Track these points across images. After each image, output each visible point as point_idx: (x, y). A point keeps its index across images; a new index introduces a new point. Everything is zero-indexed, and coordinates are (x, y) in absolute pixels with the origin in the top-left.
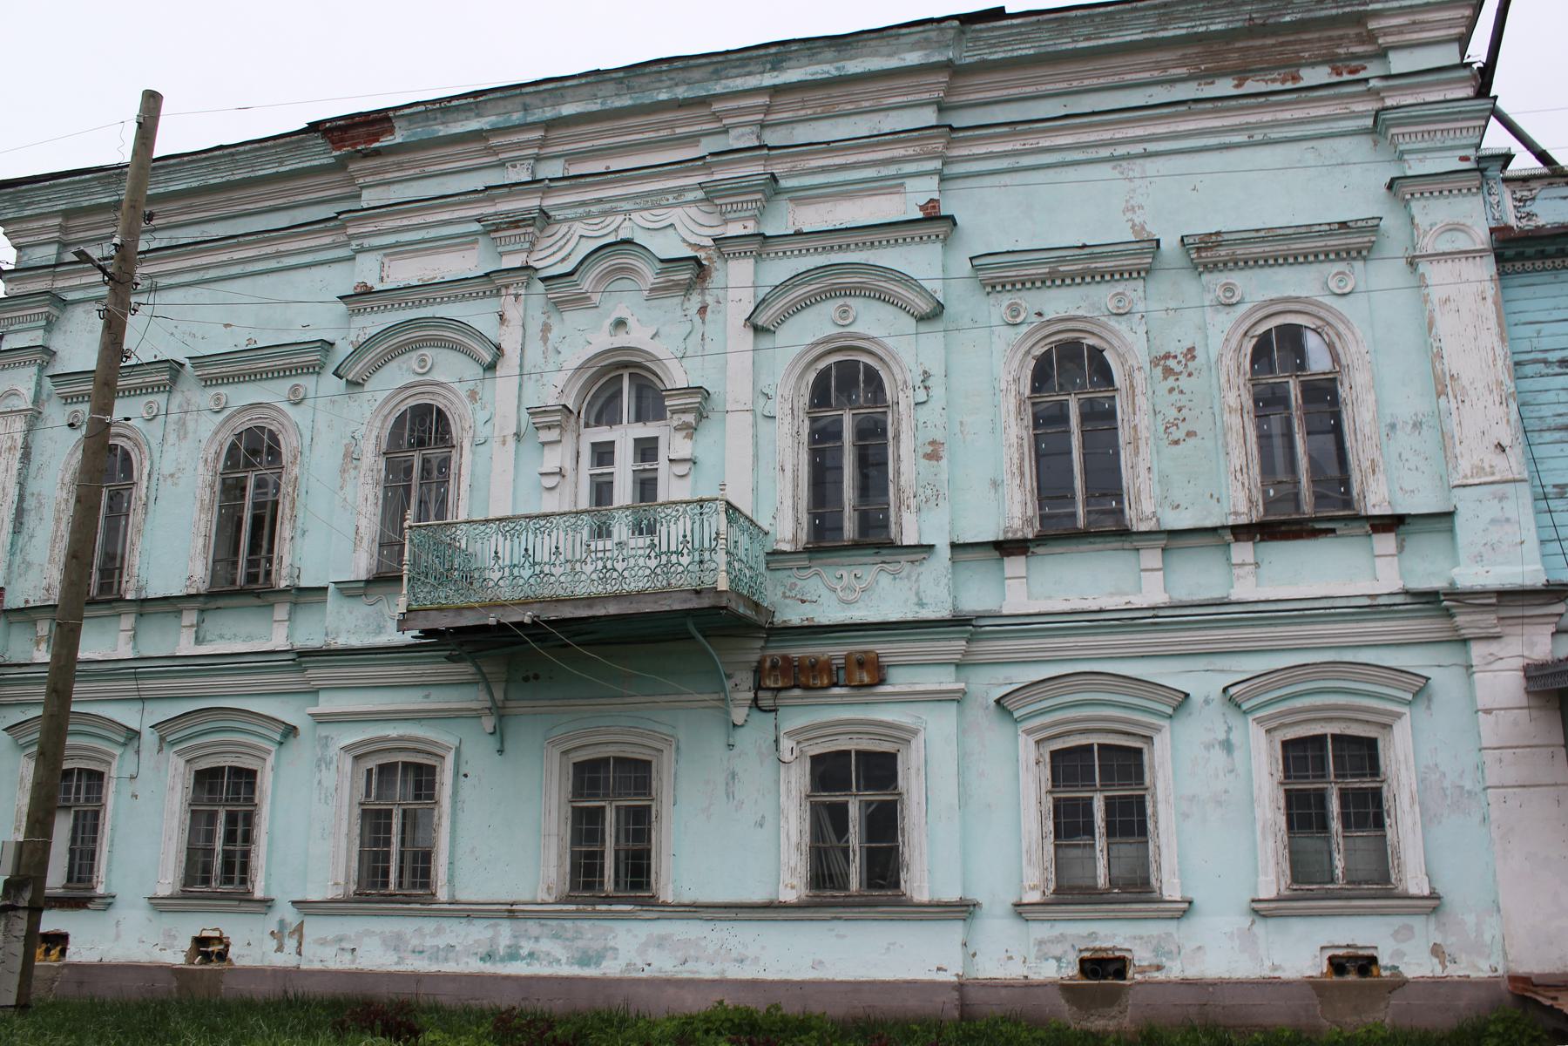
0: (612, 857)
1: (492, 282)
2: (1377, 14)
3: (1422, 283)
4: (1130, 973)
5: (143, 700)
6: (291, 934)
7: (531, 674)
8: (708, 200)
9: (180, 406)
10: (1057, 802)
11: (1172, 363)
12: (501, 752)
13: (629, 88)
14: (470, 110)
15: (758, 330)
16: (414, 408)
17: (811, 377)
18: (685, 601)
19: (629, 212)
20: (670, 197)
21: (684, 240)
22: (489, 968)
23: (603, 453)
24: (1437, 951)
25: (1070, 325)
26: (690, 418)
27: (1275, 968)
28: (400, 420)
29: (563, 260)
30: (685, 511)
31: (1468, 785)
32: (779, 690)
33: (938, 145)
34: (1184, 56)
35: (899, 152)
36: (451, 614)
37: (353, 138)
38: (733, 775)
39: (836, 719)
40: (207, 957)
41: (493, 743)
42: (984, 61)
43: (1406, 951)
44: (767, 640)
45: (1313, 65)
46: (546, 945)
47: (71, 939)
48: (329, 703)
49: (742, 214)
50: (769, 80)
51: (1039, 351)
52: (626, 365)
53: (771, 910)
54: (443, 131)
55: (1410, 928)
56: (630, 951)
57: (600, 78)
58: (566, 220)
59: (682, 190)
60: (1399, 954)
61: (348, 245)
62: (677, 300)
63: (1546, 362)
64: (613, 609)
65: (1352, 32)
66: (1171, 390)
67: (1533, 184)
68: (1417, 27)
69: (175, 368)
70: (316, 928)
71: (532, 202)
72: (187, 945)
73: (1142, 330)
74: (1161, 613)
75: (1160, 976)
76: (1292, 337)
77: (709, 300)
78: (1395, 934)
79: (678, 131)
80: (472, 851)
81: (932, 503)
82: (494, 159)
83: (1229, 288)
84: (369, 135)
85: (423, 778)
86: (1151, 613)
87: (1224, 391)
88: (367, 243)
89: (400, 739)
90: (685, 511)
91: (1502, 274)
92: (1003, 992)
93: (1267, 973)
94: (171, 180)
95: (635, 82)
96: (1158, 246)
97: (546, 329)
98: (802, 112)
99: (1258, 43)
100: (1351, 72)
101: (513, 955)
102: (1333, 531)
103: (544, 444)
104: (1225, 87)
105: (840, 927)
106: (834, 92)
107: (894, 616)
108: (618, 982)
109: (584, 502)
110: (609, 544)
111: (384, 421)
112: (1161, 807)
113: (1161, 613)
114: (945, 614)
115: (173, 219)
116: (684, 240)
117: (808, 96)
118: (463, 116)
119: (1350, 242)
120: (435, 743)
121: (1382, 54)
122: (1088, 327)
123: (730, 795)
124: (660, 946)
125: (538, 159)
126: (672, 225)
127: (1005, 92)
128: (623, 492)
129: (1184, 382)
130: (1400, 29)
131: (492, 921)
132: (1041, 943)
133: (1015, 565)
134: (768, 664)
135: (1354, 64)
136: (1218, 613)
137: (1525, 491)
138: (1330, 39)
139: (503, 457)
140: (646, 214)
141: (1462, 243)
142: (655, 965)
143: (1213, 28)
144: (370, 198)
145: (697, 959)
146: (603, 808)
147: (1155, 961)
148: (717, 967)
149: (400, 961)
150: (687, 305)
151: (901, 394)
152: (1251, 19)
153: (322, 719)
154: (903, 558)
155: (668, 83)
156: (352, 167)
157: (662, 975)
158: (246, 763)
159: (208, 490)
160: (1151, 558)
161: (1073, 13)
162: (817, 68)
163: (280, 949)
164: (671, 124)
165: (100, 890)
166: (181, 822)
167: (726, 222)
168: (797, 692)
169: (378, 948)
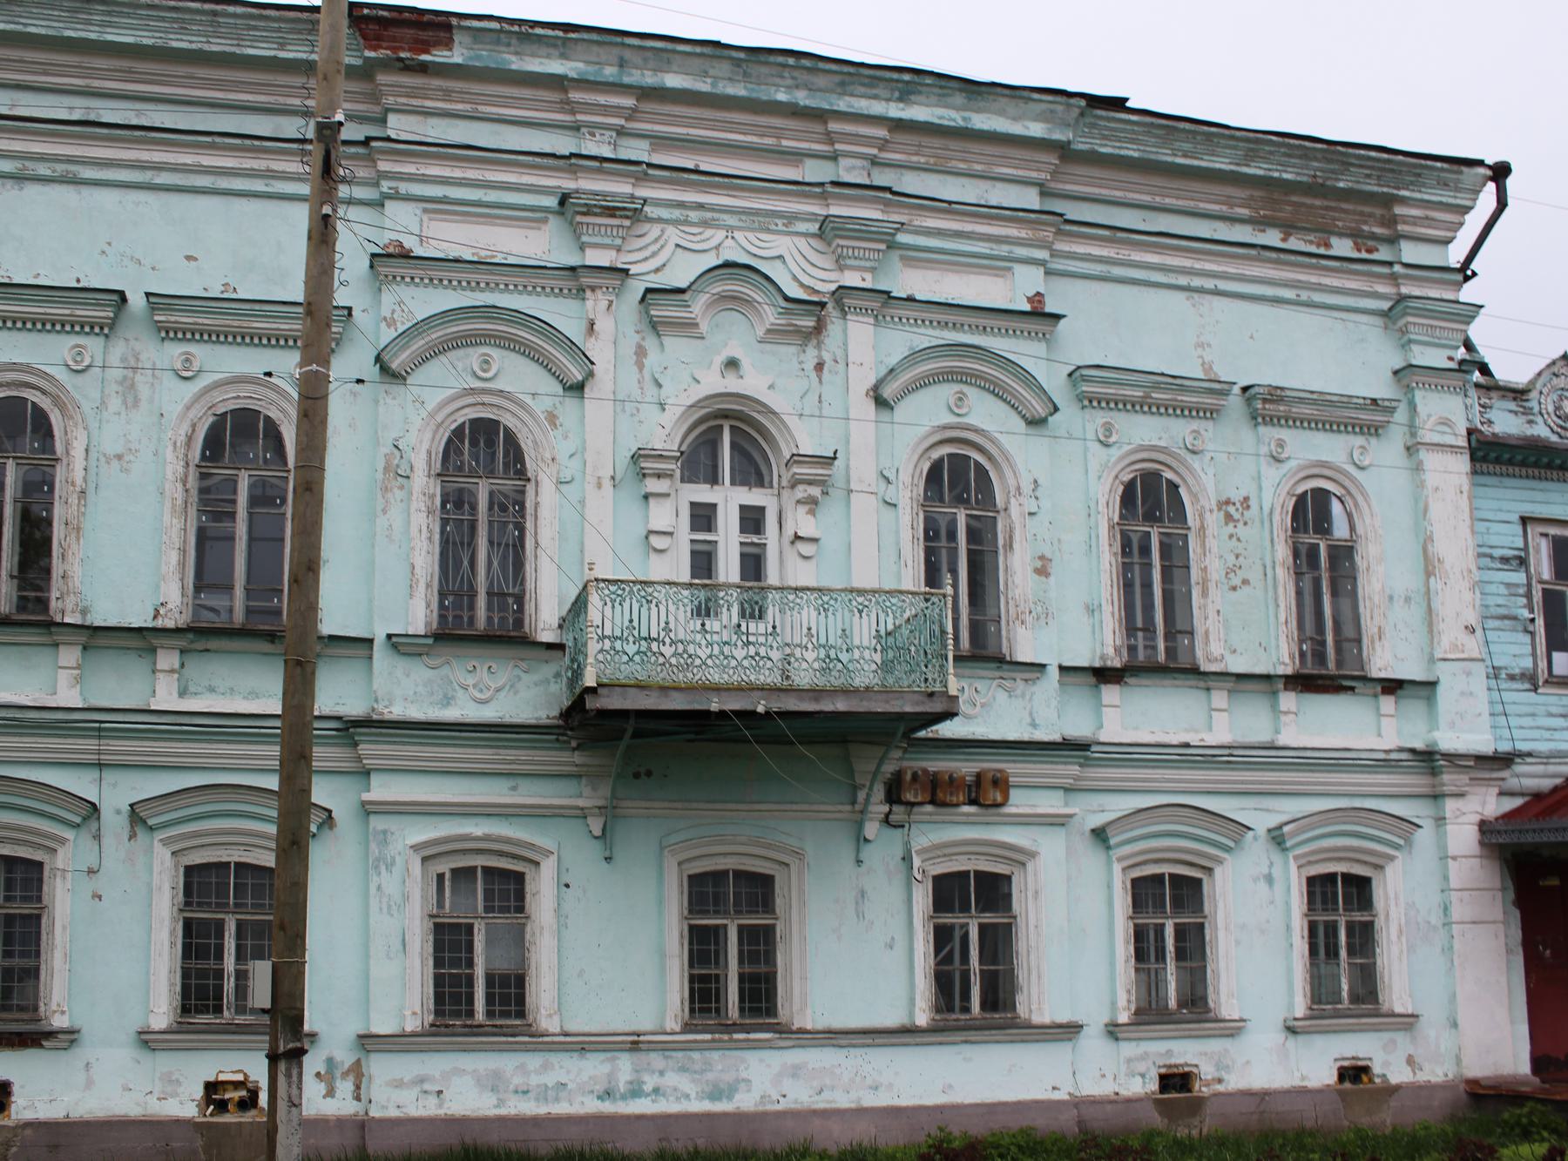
0: (733, 979)
1: (577, 278)
2: (1403, 201)
3: (1418, 468)
4: (1197, 1087)
5: (100, 766)
6: (345, 1075)
7: (642, 770)
8: (820, 235)
9: (124, 359)
10: (691, 927)
11: (1231, 509)
12: (608, 859)
13: (745, 74)
14: (555, 46)
15: (881, 402)
16: (475, 422)
17: (926, 466)
18: (917, 704)
19: (730, 229)
20: (779, 222)
21: (795, 278)
22: (608, 1107)
23: (703, 517)
24: (1410, 1061)
25: (1162, 457)
26: (815, 491)
27: (1303, 1078)
28: (458, 432)
29: (657, 270)
30: (631, 591)
31: (1433, 922)
32: (913, 804)
33: (1048, 234)
34: (1251, 198)
35: (1012, 232)
36: (655, 694)
37: (394, 39)
38: (863, 894)
39: (952, 839)
40: (222, 1106)
41: (595, 850)
42: (1094, 153)
43: (1391, 1062)
44: (905, 751)
45: (1341, 235)
46: (672, 1079)
47: (15, 1089)
48: (383, 789)
49: (862, 263)
50: (895, 111)
51: (1127, 477)
52: (725, 415)
53: (906, 1034)
54: (517, 63)
55: (1393, 1042)
56: (762, 1081)
57: (718, 52)
58: (660, 220)
59: (792, 218)
60: (1386, 1064)
61: (377, 185)
62: (793, 349)
63: (1491, 557)
64: (841, 706)
65: (1378, 212)
66: (1231, 536)
67: (1494, 394)
68: (1426, 222)
69: (1220, 389)
70: (382, 1068)
71: (621, 187)
72: (199, 1092)
73: (1211, 472)
74: (1236, 752)
75: (1220, 1088)
76: (1322, 497)
77: (826, 356)
78: (1384, 1048)
79: (785, 143)
80: (581, 974)
81: (1043, 621)
82: (568, 118)
83: (1281, 444)
84: (417, 41)
85: (507, 889)
86: (1226, 752)
87: (1268, 546)
88: (404, 188)
89: (487, 838)
90: (631, 591)
91: (1474, 472)
92: (1109, 1107)
93: (1297, 1083)
94: (110, 25)
95: (756, 70)
96: (350, 315)
97: (641, 352)
98: (915, 159)
99: (1308, 201)
100: (1369, 251)
101: (635, 1092)
102: (1352, 689)
103: (646, 497)
104: (1272, 237)
105: (967, 1050)
106: (953, 144)
107: (1012, 736)
108: (763, 1116)
109: (685, 576)
110: (761, 628)
111: (435, 432)
112: (1221, 934)
113: (1236, 752)
114: (1057, 737)
115: (96, 83)
116: (795, 278)
117: (926, 141)
118: (544, 50)
119: (1361, 418)
120: (531, 846)
121: (1393, 240)
122: (1169, 460)
123: (860, 915)
124: (794, 1076)
125: (621, 132)
126: (780, 257)
127: (1096, 191)
128: (728, 568)
129: (1241, 530)
130: (1415, 221)
131: (609, 1055)
132: (1129, 1061)
133: (1110, 693)
134: (908, 777)
135: (1371, 243)
136: (1270, 756)
137: (1480, 670)
138: (1362, 214)
139: (603, 507)
140: (750, 236)
141: (1449, 440)
142: (791, 1096)
143: (1285, 176)
144: (399, 126)
145: (833, 1088)
146: (725, 926)
147: (1217, 1075)
148: (853, 1095)
149: (501, 1103)
150: (802, 357)
151: (1013, 500)
152: (1315, 176)
153: (368, 810)
154: (1019, 676)
155: (789, 82)
156: (382, 78)
157: (798, 1106)
158: (37, 856)
159: (179, 486)
160: (1219, 698)
161: (1182, 125)
162: (940, 111)
163: (330, 1093)
164: (778, 133)
165: (59, 1022)
166: (172, 932)
167: (841, 268)
168: (929, 808)
169: (468, 1086)
